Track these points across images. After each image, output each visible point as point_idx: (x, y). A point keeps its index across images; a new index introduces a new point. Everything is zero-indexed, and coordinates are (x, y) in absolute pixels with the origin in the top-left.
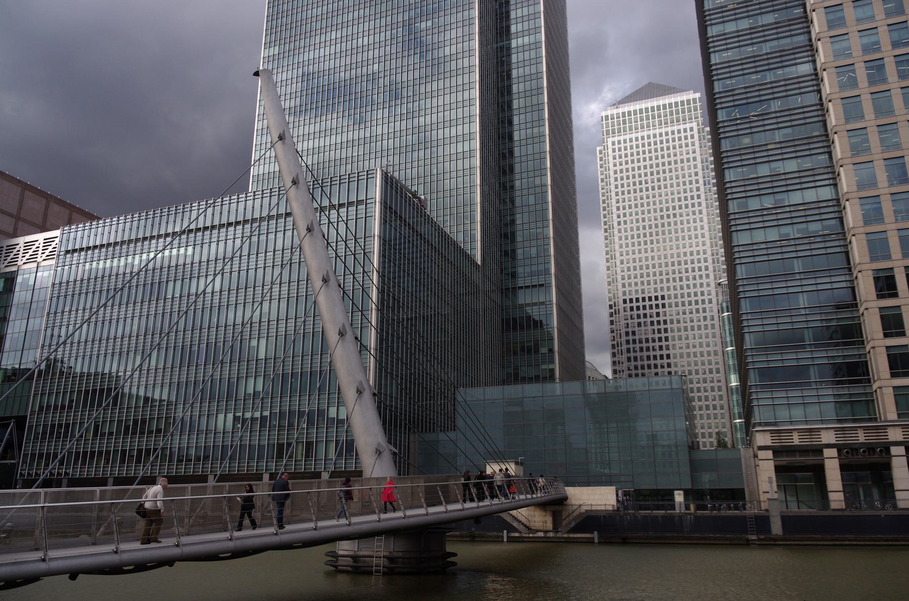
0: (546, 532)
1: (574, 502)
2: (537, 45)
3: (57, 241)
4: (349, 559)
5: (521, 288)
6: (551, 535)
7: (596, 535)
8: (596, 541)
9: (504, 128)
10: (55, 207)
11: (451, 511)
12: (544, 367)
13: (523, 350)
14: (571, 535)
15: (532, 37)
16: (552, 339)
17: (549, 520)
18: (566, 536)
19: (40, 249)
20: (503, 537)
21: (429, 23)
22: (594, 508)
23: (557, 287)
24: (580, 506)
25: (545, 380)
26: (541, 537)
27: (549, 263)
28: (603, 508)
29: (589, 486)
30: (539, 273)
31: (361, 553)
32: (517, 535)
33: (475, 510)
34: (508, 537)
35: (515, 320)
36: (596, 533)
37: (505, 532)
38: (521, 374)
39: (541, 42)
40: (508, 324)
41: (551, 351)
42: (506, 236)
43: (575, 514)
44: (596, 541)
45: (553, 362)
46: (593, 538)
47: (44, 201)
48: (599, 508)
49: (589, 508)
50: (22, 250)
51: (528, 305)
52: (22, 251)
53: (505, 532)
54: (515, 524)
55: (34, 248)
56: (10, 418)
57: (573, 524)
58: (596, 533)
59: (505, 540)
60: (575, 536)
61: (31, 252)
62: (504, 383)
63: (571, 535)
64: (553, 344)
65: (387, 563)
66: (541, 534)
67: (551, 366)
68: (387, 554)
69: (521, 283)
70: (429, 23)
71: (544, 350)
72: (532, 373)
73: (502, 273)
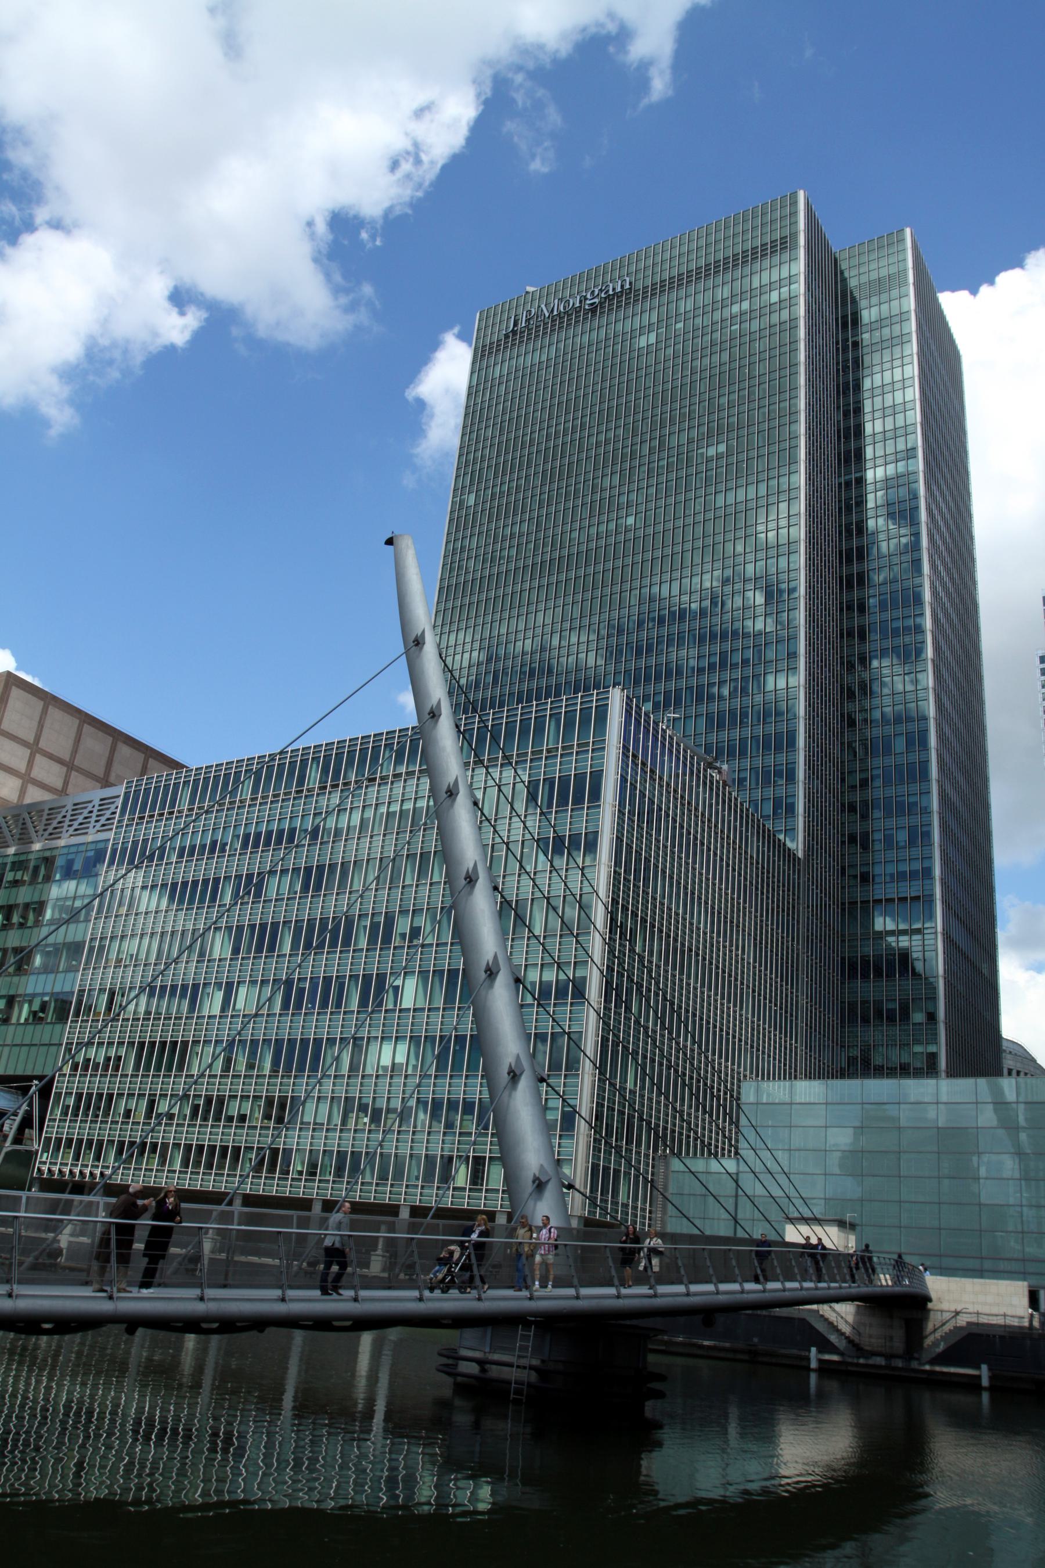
0: (889, 1357)
1: (945, 1306)
2: (792, 299)
3: (120, 802)
4: (474, 1364)
5: (878, 901)
6: (900, 1363)
7: (984, 1371)
8: (985, 1382)
9: (851, 618)
10: (124, 750)
11: (696, 1294)
12: (918, 1049)
13: (879, 1013)
14: (938, 1369)
15: (785, 290)
16: (933, 998)
17: (898, 1334)
18: (927, 1367)
19: (94, 815)
20: (808, 1359)
21: (722, 448)
22: (984, 1320)
23: (945, 901)
24: (957, 1313)
25: (918, 1073)
26: (880, 1367)
27: (931, 858)
28: (1000, 1321)
29: (982, 1277)
30: (913, 875)
31: (496, 1357)
32: (835, 1358)
33: (738, 1296)
34: (820, 1361)
35: (865, 962)
36: (984, 1367)
37: (813, 1350)
38: (877, 1060)
39: (916, 473)
40: (853, 966)
41: (932, 1017)
42: (852, 808)
43: (947, 1328)
44: (985, 1382)
45: (935, 1040)
46: (979, 1377)
47: (109, 740)
48: (994, 1321)
49: (974, 1319)
50: (93, 824)
51: (892, 933)
52: (69, 818)
53: (813, 1350)
54: (833, 1338)
55: (85, 813)
56: (30, 1078)
57: (942, 1347)
58: (984, 1367)
59: (814, 1365)
60: (945, 1369)
61: (80, 819)
62: (843, 1074)
63: (938, 1369)
64: (935, 1006)
65: (534, 1377)
66: (880, 1361)
67: (932, 1049)
68: (535, 1362)
69: (879, 892)
70: (722, 448)
71: (918, 1017)
72: (897, 1056)
73: (843, 874)
